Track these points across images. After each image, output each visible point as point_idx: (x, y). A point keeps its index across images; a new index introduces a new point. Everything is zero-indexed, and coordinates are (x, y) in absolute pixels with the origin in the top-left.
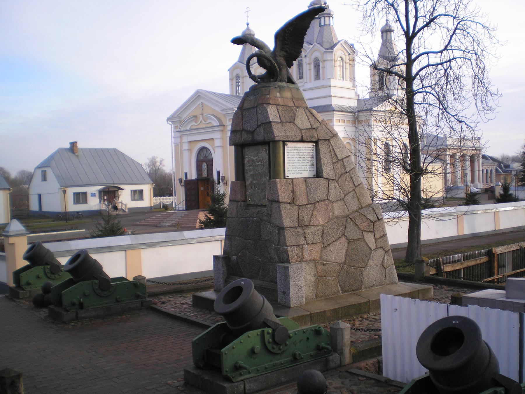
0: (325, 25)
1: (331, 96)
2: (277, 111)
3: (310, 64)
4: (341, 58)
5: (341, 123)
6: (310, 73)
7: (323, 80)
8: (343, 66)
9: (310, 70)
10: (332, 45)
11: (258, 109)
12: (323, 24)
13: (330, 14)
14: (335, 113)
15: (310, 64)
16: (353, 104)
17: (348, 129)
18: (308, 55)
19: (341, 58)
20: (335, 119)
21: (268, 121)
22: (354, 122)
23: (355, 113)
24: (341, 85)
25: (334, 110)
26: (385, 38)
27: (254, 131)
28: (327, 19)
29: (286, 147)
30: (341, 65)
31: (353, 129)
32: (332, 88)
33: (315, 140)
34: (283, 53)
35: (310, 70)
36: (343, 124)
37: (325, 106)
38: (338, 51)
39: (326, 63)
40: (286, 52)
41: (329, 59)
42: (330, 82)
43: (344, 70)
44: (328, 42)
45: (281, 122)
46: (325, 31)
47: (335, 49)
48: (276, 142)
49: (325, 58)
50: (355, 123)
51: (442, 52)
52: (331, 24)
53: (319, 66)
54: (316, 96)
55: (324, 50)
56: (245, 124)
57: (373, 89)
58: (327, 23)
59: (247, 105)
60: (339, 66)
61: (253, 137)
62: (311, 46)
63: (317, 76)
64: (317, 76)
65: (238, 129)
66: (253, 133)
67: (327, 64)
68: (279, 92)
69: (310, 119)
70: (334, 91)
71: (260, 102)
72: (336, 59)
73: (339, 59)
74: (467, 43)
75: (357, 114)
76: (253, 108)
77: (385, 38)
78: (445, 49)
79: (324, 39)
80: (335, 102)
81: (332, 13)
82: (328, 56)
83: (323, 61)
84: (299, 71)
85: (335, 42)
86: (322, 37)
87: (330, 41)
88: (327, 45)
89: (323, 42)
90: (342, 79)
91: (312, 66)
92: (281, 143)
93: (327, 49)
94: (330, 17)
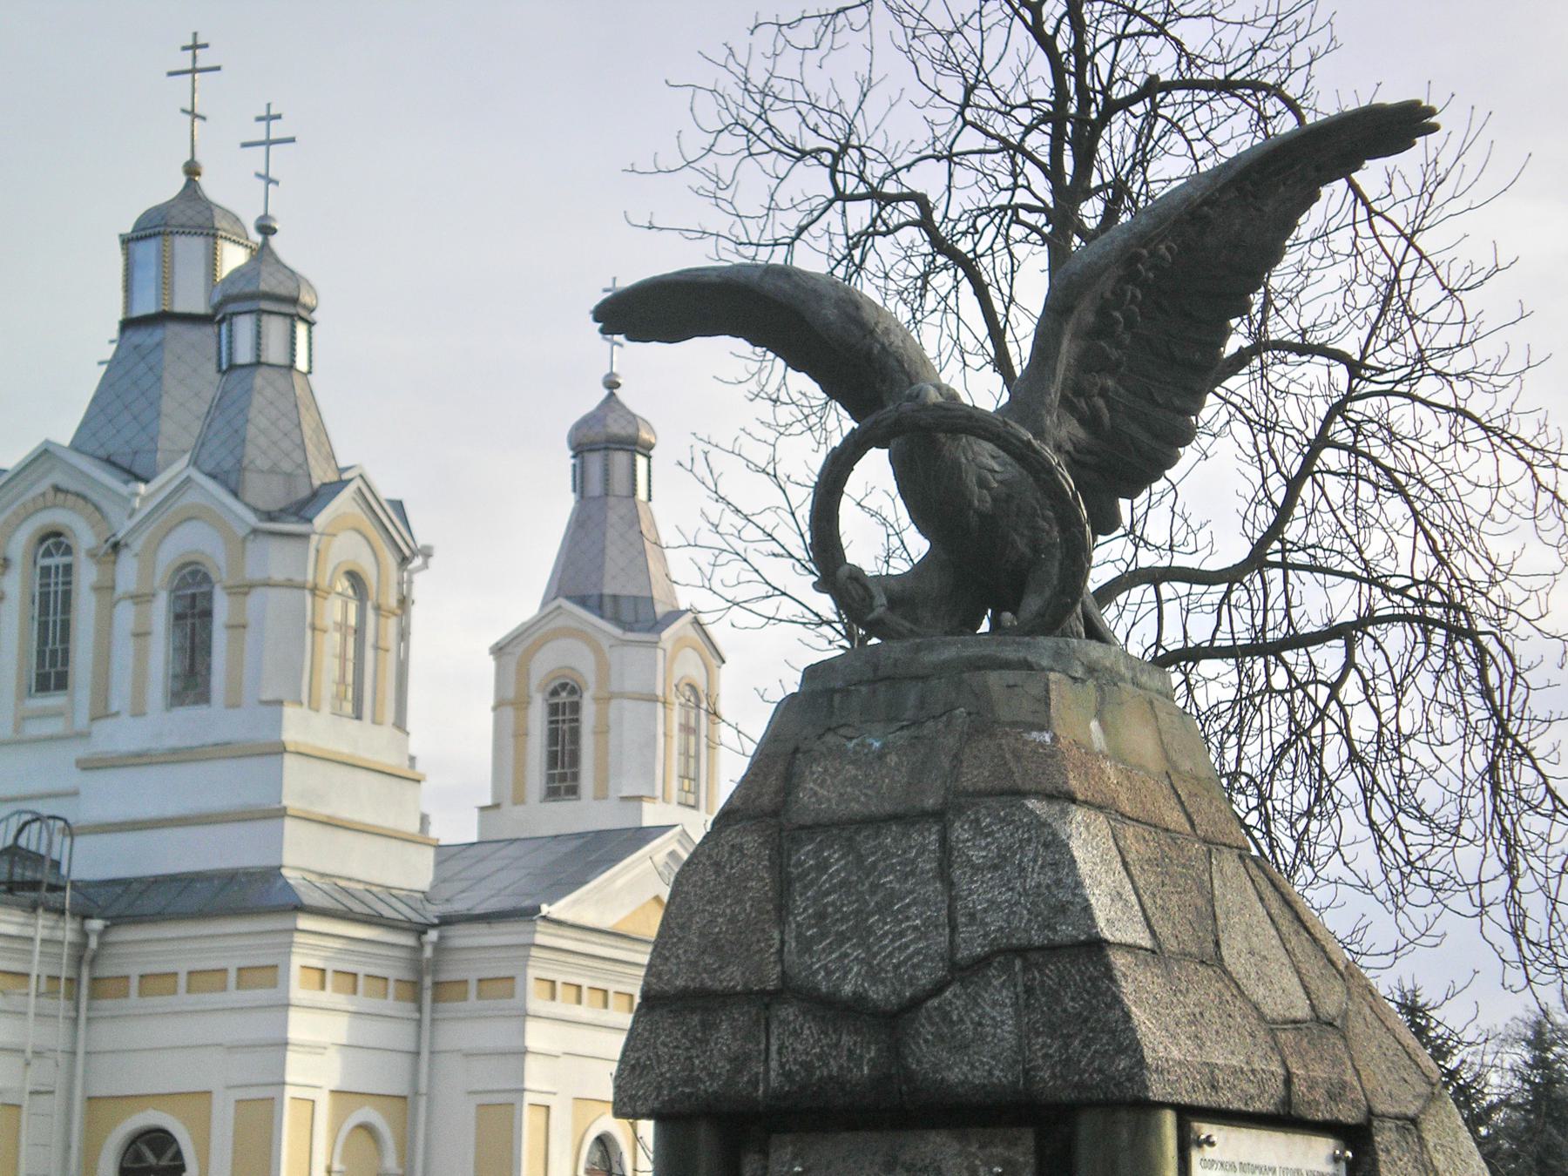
0: (258, 363)
1: (281, 813)
2: (1119, 867)
3: (141, 599)
4: (355, 578)
5: (329, 997)
6: (141, 657)
7: (233, 704)
8: (359, 631)
9: (141, 635)
10: (304, 493)
11: (961, 832)
12: (244, 355)
13: (294, 301)
14: (304, 922)
15: (141, 599)
16: (412, 872)
17: (378, 1033)
18: (137, 544)
19: (355, 578)
20: (297, 961)
21: (1066, 931)
22: (413, 990)
23: (420, 930)
24: (343, 748)
25: (300, 908)
26: (595, 488)
27: (916, 1003)
28: (275, 328)
29: (1196, 1156)
30: (352, 621)
31: (401, 1035)
32: (289, 760)
33: (1348, 1114)
34: (1069, 430)
35: (141, 635)
36: (341, 1000)
37: (231, 878)
38: (339, 537)
39: (254, 599)
40: (1090, 421)
41: (278, 576)
42: (278, 723)
43: (369, 654)
44: (273, 470)
45: (1156, 952)
46: (258, 401)
47: (320, 521)
48: (1148, 1107)
49: (252, 572)
50: (417, 999)
51: (1231, 576)
52: (301, 364)
53: (207, 614)
54: (171, 810)
55: (252, 519)
56: (806, 945)
57: (508, 790)
58: (274, 352)
59: (820, 792)
60: (342, 626)
61: (895, 1051)
62: (142, 488)
63: (191, 681)
64: (191, 681)
65: (733, 977)
66: (892, 1021)
67: (267, 607)
68: (1099, 715)
69: (1294, 942)
70: (298, 784)
71: (974, 776)
72: (324, 583)
73: (343, 585)
74: (1397, 549)
75: (433, 935)
76: (906, 819)
77: (595, 488)
78: (1257, 560)
79: (251, 452)
80: (303, 856)
81: (306, 298)
82: (275, 560)
83: (242, 590)
84: (43, 640)
85: (321, 475)
86: (238, 438)
87: (286, 466)
88: (269, 493)
89: (240, 468)
90: (348, 707)
91: (160, 612)
92: (1169, 1119)
93: (270, 516)
94: (293, 318)
